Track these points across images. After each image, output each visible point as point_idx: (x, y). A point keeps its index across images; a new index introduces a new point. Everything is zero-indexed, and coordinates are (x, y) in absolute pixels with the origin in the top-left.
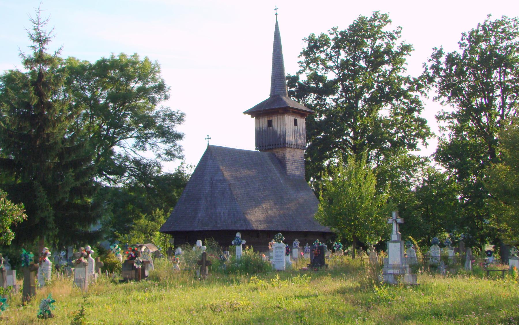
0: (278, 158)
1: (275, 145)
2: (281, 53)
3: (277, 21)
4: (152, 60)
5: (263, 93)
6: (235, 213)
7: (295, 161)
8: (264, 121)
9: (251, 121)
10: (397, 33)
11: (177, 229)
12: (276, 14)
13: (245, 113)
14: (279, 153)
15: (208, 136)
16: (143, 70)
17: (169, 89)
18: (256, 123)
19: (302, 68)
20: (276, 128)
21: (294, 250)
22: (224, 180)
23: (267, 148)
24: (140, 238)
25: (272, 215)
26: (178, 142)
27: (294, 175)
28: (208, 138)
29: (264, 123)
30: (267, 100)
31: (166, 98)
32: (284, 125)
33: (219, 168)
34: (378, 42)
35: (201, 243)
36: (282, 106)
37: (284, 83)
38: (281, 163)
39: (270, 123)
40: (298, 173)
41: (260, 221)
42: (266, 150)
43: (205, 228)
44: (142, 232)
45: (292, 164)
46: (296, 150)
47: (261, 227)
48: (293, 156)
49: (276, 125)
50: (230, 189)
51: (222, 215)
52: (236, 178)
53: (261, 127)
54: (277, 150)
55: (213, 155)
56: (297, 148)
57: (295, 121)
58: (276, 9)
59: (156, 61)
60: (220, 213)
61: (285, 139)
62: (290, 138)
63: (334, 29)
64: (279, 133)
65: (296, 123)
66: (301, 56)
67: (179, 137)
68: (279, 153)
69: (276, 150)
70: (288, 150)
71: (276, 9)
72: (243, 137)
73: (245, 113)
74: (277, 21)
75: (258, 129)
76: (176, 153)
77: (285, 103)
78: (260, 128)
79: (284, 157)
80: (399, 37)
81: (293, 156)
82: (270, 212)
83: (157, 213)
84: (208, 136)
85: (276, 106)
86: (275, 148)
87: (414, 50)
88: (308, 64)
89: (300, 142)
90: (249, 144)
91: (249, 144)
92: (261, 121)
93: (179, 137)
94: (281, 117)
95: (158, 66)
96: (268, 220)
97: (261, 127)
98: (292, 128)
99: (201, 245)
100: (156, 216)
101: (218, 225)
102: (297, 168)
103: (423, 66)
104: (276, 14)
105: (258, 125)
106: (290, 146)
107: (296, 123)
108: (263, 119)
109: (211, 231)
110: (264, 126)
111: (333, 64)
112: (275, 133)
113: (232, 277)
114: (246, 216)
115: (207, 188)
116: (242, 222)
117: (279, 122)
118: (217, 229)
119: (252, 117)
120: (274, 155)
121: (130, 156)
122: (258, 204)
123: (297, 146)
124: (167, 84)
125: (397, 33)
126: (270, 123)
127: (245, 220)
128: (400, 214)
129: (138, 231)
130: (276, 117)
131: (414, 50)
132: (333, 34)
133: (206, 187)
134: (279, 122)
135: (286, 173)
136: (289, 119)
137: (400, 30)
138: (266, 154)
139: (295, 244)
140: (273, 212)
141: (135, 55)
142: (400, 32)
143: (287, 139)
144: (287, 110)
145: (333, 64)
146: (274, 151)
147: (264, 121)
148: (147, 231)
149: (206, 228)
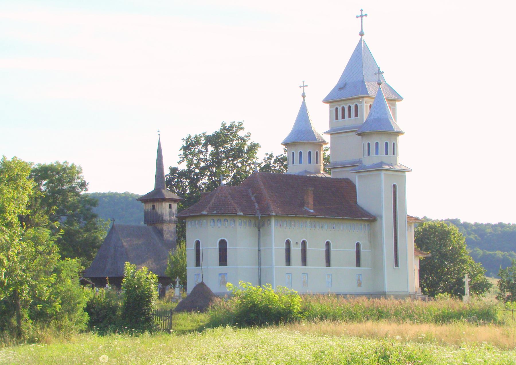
4: (77, 164)
7: (169, 231)
8: (149, 206)
10: (247, 137)
11: (94, 276)
14: (159, 226)
19: (182, 159)
22: (123, 246)
26: (94, 220)
32: (162, 208)
36: (161, 197)
38: (160, 233)
39: (154, 207)
40: (171, 239)
42: (151, 224)
54: (158, 225)
61: (163, 218)
62: (166, 217)
65: (170, 207)
66: (181, 149)
68: (159, 226)
77: (163, 195)
79: (162, 229)
80: (249, 139)
85: (157, 197)
88: (186, 156)
102: (171, 236)
106: (166, 222)
107: (170, 207)
113: (42, 168)
120: (156, 227)
123: (171, 221)
125: (247, 137)
126: (154, 207)
128: (61, 300)
136: (166, 205)
138: (150, 227)
141: (66, 162)
142: (250, 136)
143: (165, 218)
144: (164, 200)
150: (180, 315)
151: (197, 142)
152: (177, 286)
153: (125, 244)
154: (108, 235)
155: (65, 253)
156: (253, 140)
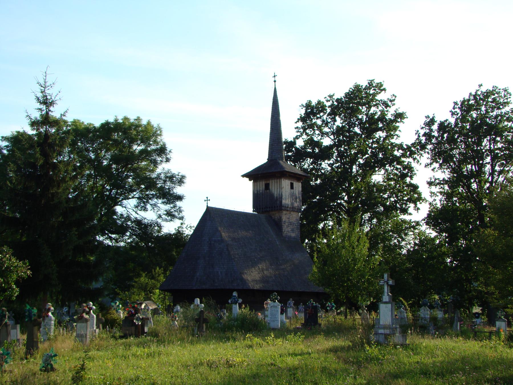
3: (275, 88)
5: (260, 157)
7: (291, 223)
8: (262, 185)
9: (249, 185)
10: (391, 101)
12: (275, 81)
13: (243, 176)
14: (276, 215)
16: (146, 133)
17: (170, 152)
19: (299, 134)
20: (273, 191)
21: (289, 309)
22: (222, 241)
24: (140, 296)
26: (178, 203)
27: (290, 237)
28: (207, 200)
30: (265, 164)
31: (168, 160)
32: (281, 188)
38: (278, 225)
39: (267, 186)
40: (293, 235)
41: (256, 281)
42: (263, 213)
45: (288, 226)
46: (292, 213)
47: (257, 287)
49: (273, 188)
51: (220, 274)
52: (234, 239)
54: (274, 213)
56: (293, 211)
58: (275, 76)
61: (281, 202)
62: (286, 201)
63: (331, 96)
64: (275, 196)
66: (298, 121)
67: (180, 198)
68: (276, 215)
70: (284, 212)
71: (275, 76)
73: (243, 176)
74: (275, 88)
75: (256, 192)
78: (257, 190)
79: (280, 219)
80: (394, 105)
81: (289, 218)
82: (265, 272)
92: (258, 184)
93: (180, 198)
94: (278, 180)
98: (288, 191)
100: (155, 274)
102: (293, 230)
103: (416, 134)
104: (275, 81)
106: (286, 208)
108: (261, 182)
110: (261, 189)
112: (272, 195)
114: (243, 276)
119: (250, 180)
122: (254, 264)
123: (293, 209)
124: (169, 147)
125: (391, 101)
126: (267, 186)
129: (139, 288)
130: (273, 181)
131: (407, 118)
132: (329, 101)
135: (282, 235)
136: (286, 183)
137: (394, 98)
138: (263, 216)
139: (289, 304)
142: (394, 100)
143: (284, 202)
147: (262, 185)
149: (204, 287)
150: (124, 201)
151: (320, 107)
152: (386, 298)
153: (225, 235)
154: (258, 291)
155: (414, 309)
156: (399, 106)
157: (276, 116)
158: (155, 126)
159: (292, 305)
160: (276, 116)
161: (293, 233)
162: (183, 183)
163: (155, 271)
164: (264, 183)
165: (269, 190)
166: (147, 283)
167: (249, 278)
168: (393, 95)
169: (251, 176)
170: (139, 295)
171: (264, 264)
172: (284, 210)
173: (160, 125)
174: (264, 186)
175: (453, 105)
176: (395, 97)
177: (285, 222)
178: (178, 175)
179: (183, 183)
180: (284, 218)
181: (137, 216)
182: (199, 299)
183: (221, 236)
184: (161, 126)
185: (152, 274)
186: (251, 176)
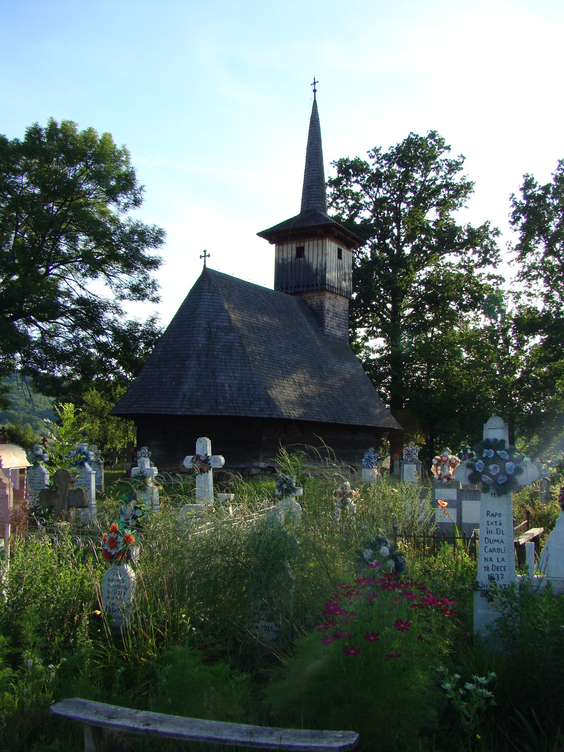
0: (310, 307)
1: (308, 286)
2: (321, 148)
5: (290, 207)
6: (251, 386)
7: (336, 314)
8: (290, 250)
9: (268, 251)
12: (315, 91)
14: (314, 300)
15: (205, 251)
17: (141, 188)
18: (278, 252)
20: (311, 260)
21: (406, 466)
22: (231, 328)
23: (293, 291)
24: (94, 425)
25: (309, 395)
26: (152, 274)
27: (334, 337)
28: (205, 255)
29: (290, 252)
31: (137, 202)
32: (324, 254)
33: (222, 307)
34: (432, 175)
35: (209, 448)
37: (323, 196)
38: (317, 315)
39: (300, 252)
41: (292, 403)
43: (196, 410)
44: (97, 416)
46: (338, 298)
47: (295, 413)
48: (334, 306)
49: (311, 255)
50: (242, 345)
51: (227, 388)
52: (251, 327)
53: (285, 257)
54: (310, 295)
55: (211, 287)
56: (340, 295)
57: (340, 252)
58: (315, 83)
59: (124, 147)
60: (223, 385)
61: (324, 277)
62: (332, 276)
63: (376, 151)
64: (314, 267)
67: (153, 263)
68: (314, 300)
69: (308, 295)
70: (328, 295)
71: (315, 83)
72: (258, 267)
75: (280, 262)
76: (148, 291)
78: (283, 259)
79: (321, 306)
81: (334, 306)
82: (304, 388)
83: (117, 391)
84: (205, 251)
86: (308, 292)
87: (474, 192)
89: (345, 284)
90: (267, 280)
91: (267, 280)
93: (153, 263)
94: (320, 242)
95: (126, 153)
96: (303, 401)
97: (285, 257)
98: (335, 263)
99: (209, 454)
100: (116, 395)
101: (220, 407)
102: (339, 326)
103: (511, 198)
104: (315, 91)
105: (281, 254)
106: (332, 290)
107: (340, 257)
108: (290, 246)
109: (207, 416)
110: (290, 256)
111: (371, 200)
112: (308, 266)
114: (270, 392)
115: (201, 340)
116: (262, 403)
117: (315, 249)
118: (218, 414)
119: (271, 242)
120: (305, 302)
121: (74, 293)
122: (286, 373)
123: (340, 292)
124: (140, 179)
126: (300, 252)
127: (269, 401)
129: (92, 413)
130: (311, 243)
131: (474, 192)
132: (373, 157)
133: (199, 339)
134: (315, 249)
135: (323, 331)
137: (461, 160)
139: (408, 454)
140: (310, 389)
143: (328, 276)
145: (371, 200)
146: (305, 295)
147: (290, 250)
148: (103, 415)
149: (197, 411)
157: (316, 142)
158: (119, 147)
159: (416, 456)
160: (316, 142)
161: (339, 330)
162: (161, 242)
163: (115, 390)
164: (294, 246)
165: (304, 257)
166: (104, 407)
167: (280, 397)
168: (462, 156)
169: (273, 235)
170: (92, 423)
171: (302, 376)
172: (328, 291)
173: (126, 147)
174: (294, 252)
175: (558, 163)
176: (464, 158)
177: (328, 310)
178: (153, 230)
179: (161, 242)
180: (327, 304)
181: (84, 293)
182: (209, 441)
183: (230, 320)
184: (128, 148)
185: (111, 394)
186: (273, 235)
